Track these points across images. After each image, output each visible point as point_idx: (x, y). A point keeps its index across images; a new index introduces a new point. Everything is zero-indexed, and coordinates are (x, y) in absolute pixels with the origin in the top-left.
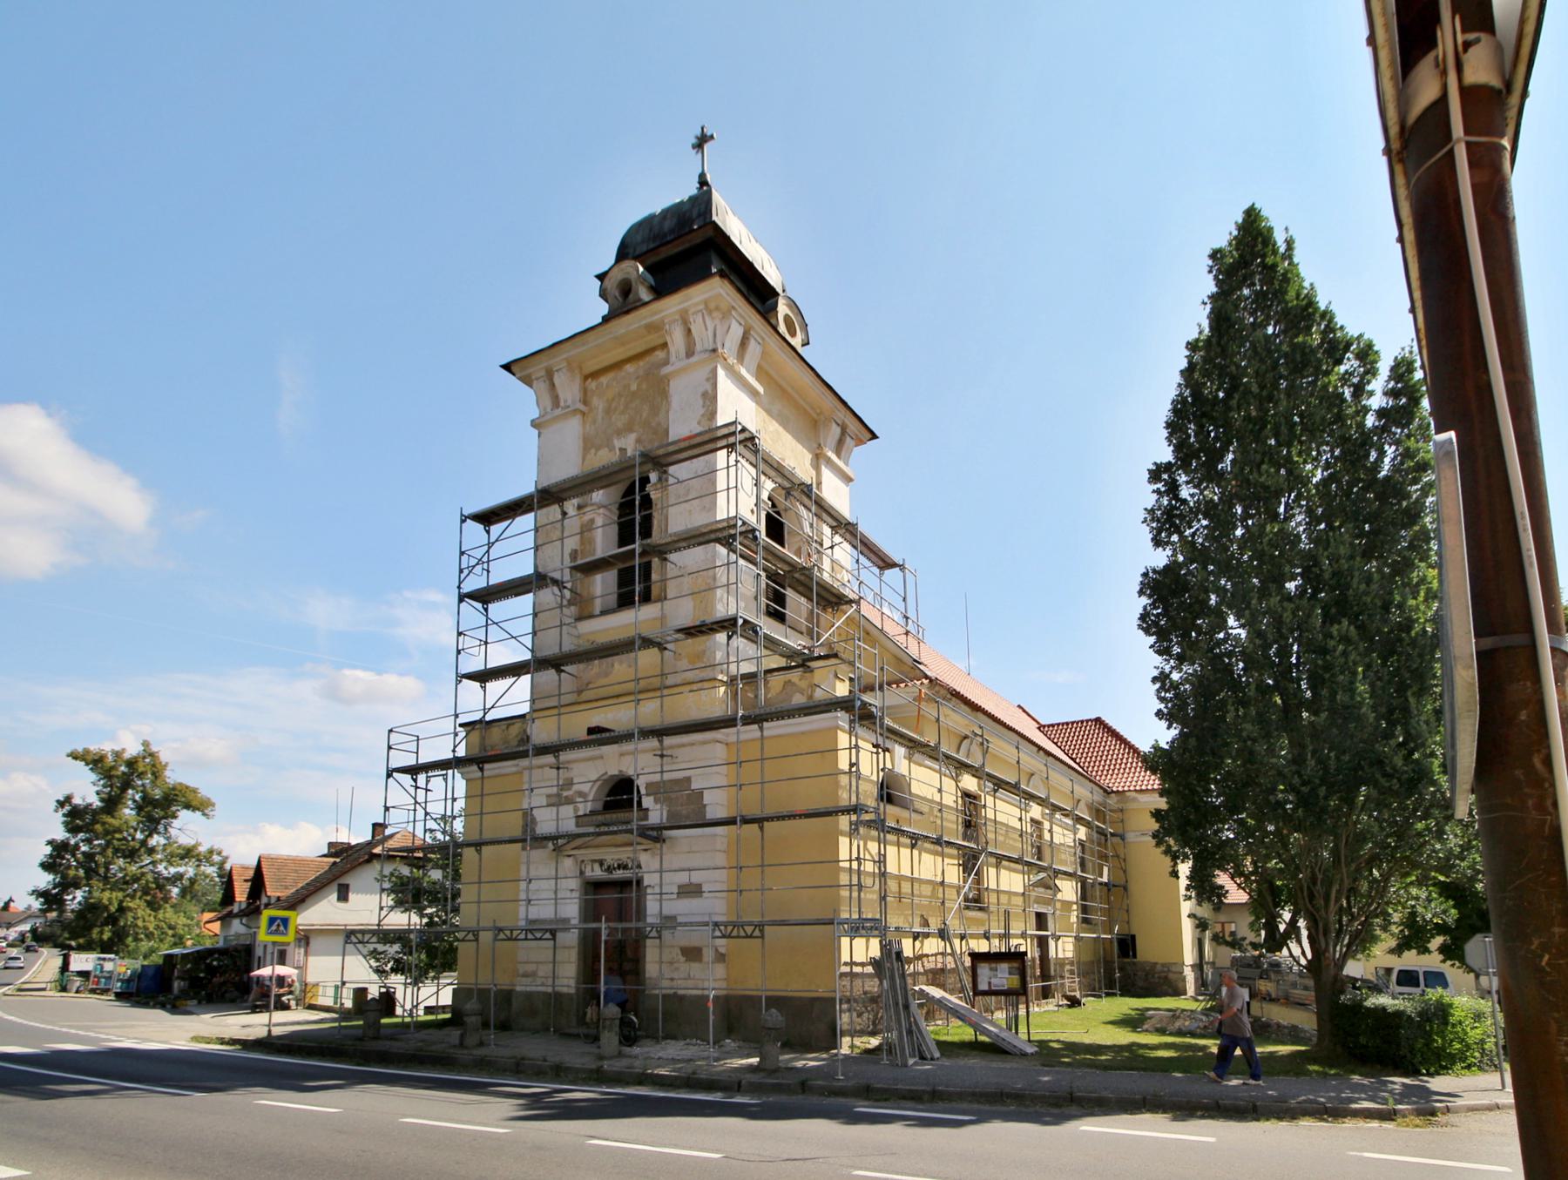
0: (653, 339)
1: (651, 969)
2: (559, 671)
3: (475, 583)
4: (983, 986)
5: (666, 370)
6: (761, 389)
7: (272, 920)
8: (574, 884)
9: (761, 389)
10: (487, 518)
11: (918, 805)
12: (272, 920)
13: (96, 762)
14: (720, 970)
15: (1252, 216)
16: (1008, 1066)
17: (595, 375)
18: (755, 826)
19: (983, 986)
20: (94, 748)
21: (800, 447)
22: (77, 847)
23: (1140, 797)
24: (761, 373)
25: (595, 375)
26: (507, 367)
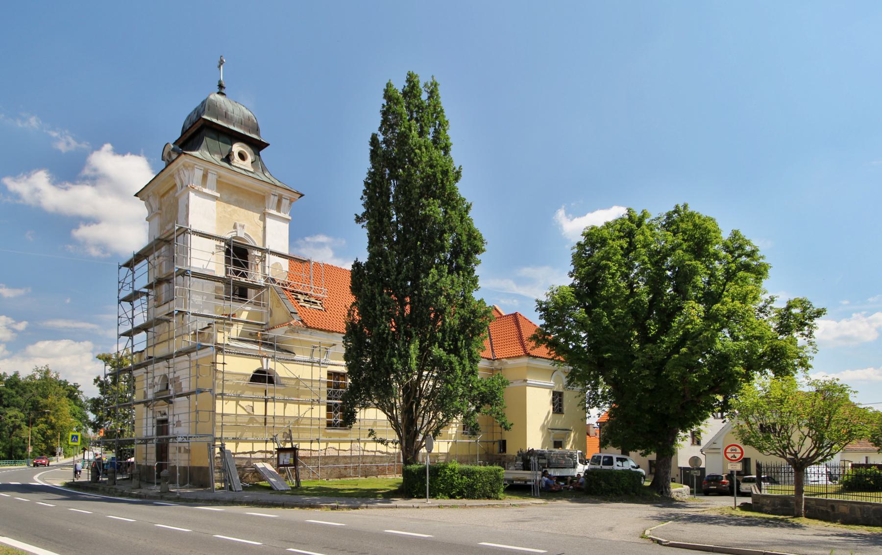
0: (171, 184)
1: (171, 456)
2: (147, 331)
3: (125, 294)
4: (281, 463)
5: (177, 194)
6: (218, 195)
7: (73, 436)
8: (150, 421)
9: (218, 195)
10: (130, 265)
11: (283, 381)
12: (73, 436)
13: (106, 359)
14: (185, 456)
15: (267, 145)
16: (817, 552)
17: (163, 196)
18: (185, 398)
19: (281, 463)
20: (106, 353)
21: (250, 213)
22: (104, 400)
23: (510, 362)
24: (219, 189)
25: (163, 196)
26: (136, 195)
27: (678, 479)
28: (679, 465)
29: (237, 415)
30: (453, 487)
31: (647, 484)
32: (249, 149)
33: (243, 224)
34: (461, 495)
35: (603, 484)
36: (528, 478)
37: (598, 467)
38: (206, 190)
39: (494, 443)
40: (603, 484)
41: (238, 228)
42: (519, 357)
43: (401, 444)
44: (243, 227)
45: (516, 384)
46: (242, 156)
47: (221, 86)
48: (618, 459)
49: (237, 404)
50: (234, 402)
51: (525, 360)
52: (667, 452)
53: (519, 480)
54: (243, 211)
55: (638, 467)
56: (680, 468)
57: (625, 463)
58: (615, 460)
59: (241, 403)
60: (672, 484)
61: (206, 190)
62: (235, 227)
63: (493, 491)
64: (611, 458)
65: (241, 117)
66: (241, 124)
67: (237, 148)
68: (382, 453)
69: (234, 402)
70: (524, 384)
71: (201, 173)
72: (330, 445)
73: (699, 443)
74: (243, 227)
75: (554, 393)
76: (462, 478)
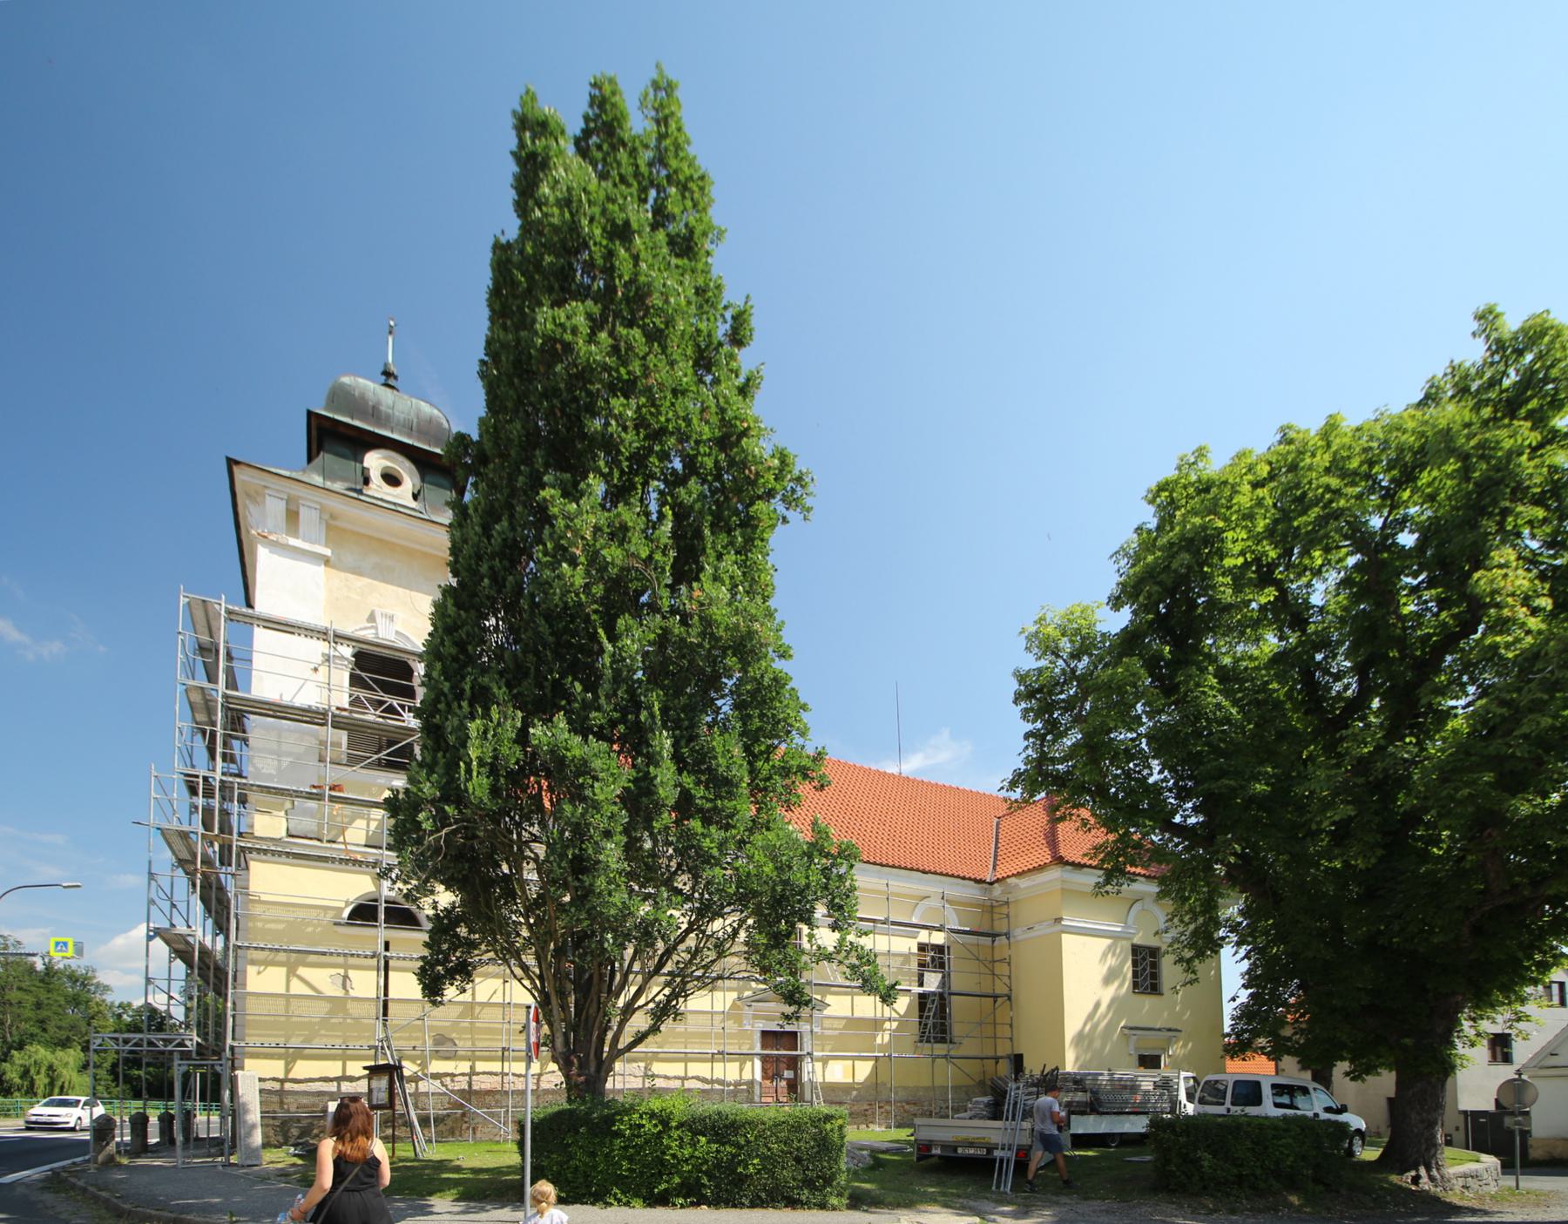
9: (328, 552)
23: (1024, 883)
27: (1459, 1136)
28: (1462, 1106)
29: (288, 997)
30: (661, 1167)
31: (1370, 1154)
32: (408, 464)
33: (390, 612)
34: (693, 1194)
35: (1207, 1161)
36: (995, 1138)
37: (1220, 1110)
38: (292, 541)
39: (997, 1059)
40: (1207, 1161)
41: (378, 619)
42: (1040, 868)
43: (553, 1047)
44: (391, 618)
45: (1040, 930)
46: (392, 479)
47: (387, 374)
48: (1278, 1089)
49: (292, 972)
50: (283, 970)
51: (1056, 873)
52: (1427, 1070)
53: (971, 1145)
54: (391, 589)
55: (1342, 1110)
56: (1465, 1112)
57: (1300, 1100)
58: (1267, 1091)
59: (302, 971)
60: (1449, 1152)
61: (292, 541)
62: (372, 618)
63: (809, 1183)
64: (1256, 1086)
65: (413, 416)
66: (409, 429)
67: (375, 461)
68: (704, 1080)
69: (283, 970)
70: (1058, 927)
71: (282, 506)
72: (481, 1066)
73: (1507, 1059)
74: (391, 618)
75: (1136, 950)
76: (694, 1144)
